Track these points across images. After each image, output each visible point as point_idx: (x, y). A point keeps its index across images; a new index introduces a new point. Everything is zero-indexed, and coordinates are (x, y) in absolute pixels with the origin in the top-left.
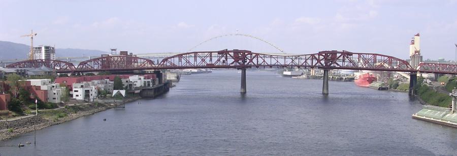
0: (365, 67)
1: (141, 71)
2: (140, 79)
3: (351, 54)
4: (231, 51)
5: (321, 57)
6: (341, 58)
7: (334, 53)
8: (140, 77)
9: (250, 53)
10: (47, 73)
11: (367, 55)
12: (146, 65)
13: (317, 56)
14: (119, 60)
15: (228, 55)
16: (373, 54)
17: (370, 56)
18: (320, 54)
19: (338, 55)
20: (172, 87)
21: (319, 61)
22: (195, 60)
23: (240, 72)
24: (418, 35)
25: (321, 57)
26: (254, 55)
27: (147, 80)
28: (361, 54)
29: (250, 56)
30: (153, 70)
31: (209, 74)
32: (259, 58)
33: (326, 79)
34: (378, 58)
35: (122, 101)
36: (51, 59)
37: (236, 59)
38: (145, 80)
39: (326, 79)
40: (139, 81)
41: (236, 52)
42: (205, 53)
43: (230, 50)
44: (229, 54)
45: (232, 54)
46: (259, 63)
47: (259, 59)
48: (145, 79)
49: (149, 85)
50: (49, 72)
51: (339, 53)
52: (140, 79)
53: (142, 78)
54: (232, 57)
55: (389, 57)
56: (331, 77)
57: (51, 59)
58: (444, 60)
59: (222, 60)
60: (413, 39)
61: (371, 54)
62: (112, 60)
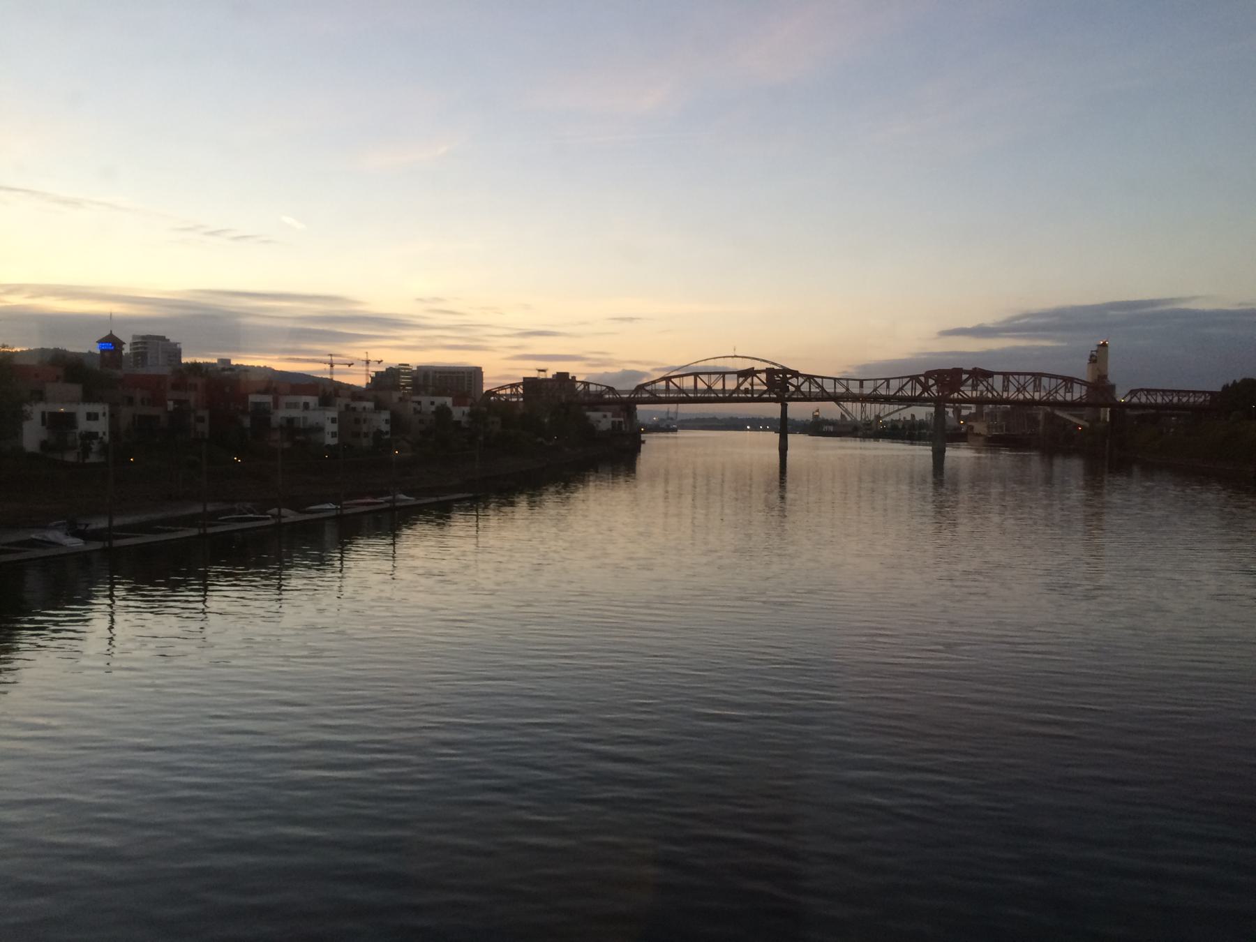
0: (990, 395)
2: (605, 416)
3: (989, 374)
4: (760, 372)
5: (931, 382)
6: (970, 382)
7: (957, 372)
13: (922, 379)
15: (671, 384)
16: (1033, 374)
18: (929, 375)
19: (965, 377)
20: (1211, 393)
21: (926, 388)
22: (1006, 388)
23: (779, 405)
25: (931, 382)
27: (617, 419)
28: (1013, 374)
36: (833, 391)
42: (878, 381)
43: (759, 369)
44: (908, 382)
51: (966, 372)
53: (609, 414)
57: (833, 391)
58: (753, 368)
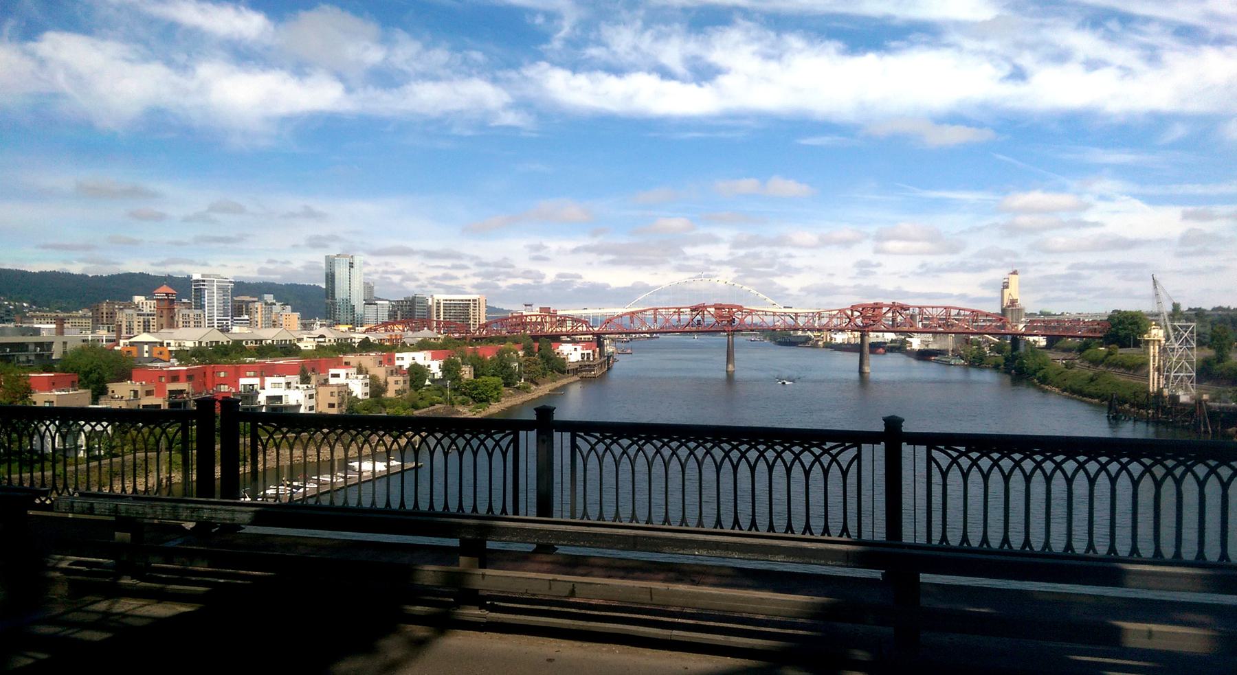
1: (573, 339)
7: (877, 307)
8: (576, 347)
9: (740, 308)
12: (580, 328)
14: (539, 320)
15: (705, 312)
17: (940, 310)
18: (853, 309)
24: (1015, 273)
27: (586, 352)
30: (591, 336)
31: (657, 340)
35: (294, 435)
40: (573, 352)
45: (712, 310)
49: (588, 358)
51: (887, 306)
53: (579, 348)
56: (516, 364)
60: (1006, 280)
61: (941, 307)
62: (528, 320)
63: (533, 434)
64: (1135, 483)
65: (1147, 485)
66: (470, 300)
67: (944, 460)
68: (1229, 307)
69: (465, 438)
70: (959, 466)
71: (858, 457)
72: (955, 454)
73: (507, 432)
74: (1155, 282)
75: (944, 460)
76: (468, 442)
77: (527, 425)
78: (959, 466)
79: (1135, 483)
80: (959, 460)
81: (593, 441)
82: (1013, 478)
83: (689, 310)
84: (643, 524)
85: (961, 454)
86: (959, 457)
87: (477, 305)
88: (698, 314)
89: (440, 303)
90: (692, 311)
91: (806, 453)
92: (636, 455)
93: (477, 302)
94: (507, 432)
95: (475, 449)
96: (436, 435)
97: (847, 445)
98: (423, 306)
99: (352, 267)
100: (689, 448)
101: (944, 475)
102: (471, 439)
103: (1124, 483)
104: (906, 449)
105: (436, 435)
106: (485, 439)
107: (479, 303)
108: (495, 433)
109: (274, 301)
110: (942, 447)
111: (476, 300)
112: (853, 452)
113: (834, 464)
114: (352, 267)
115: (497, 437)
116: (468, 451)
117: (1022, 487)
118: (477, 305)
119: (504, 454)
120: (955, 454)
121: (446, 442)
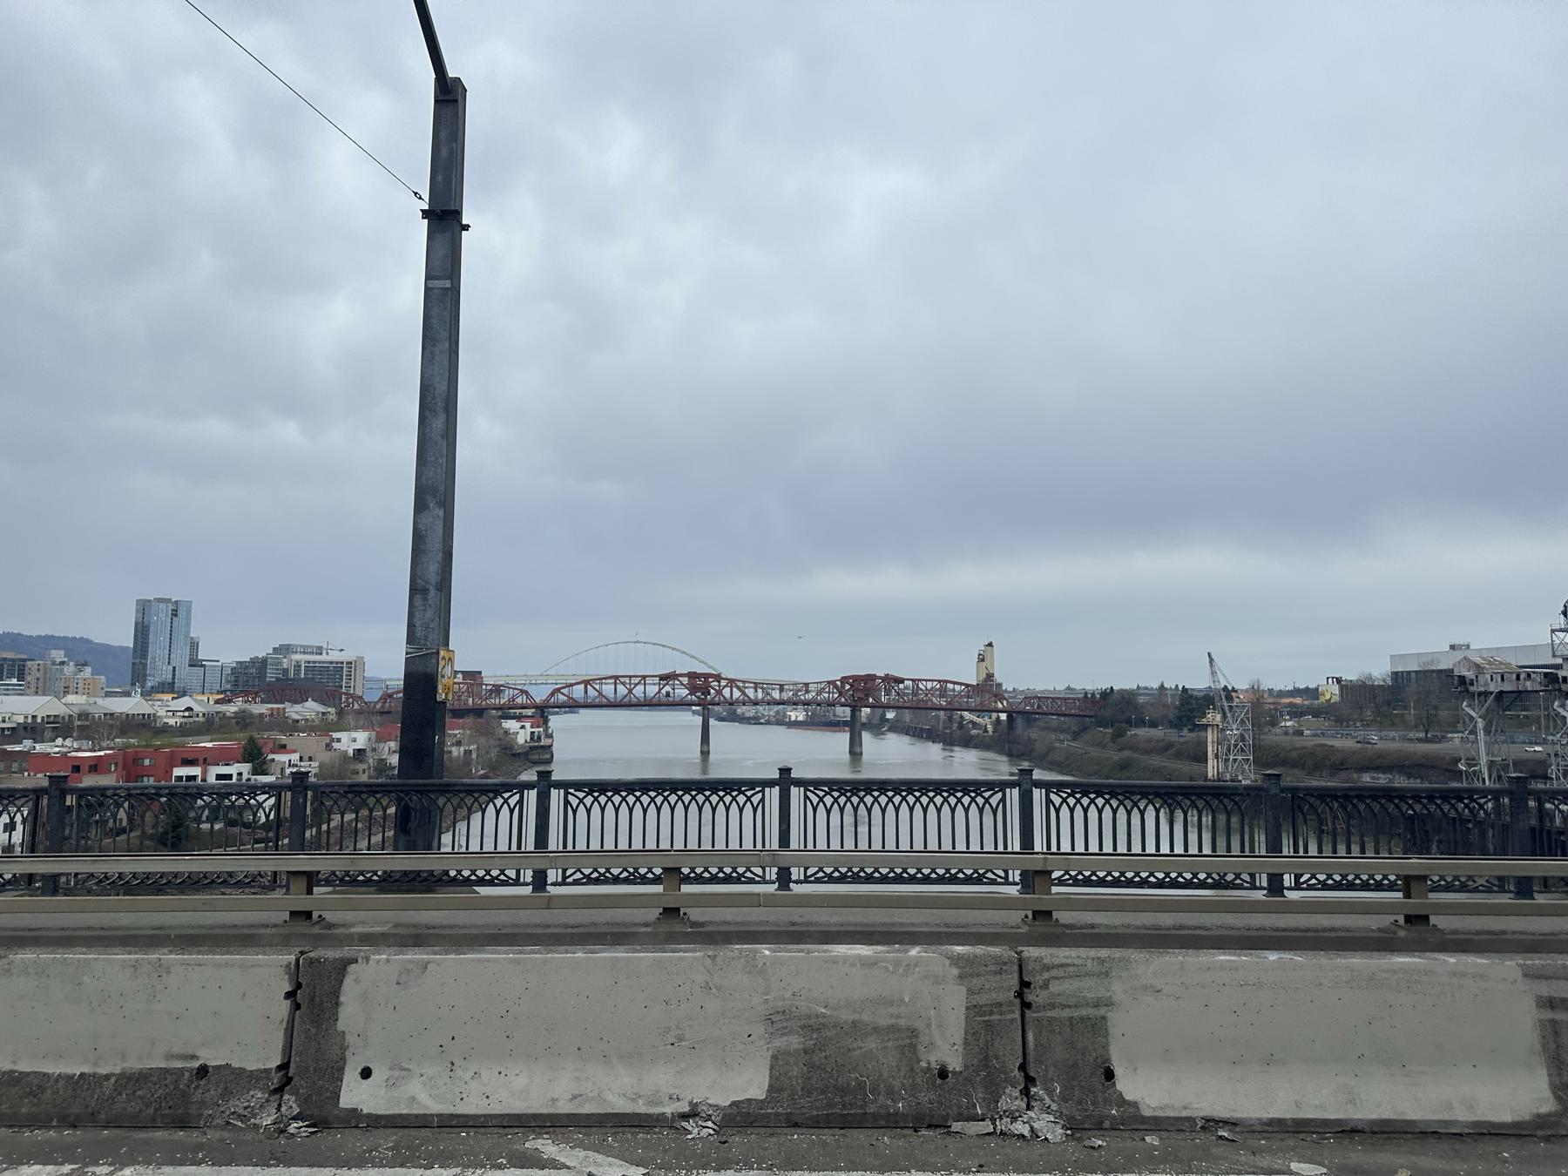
4: (681, 675)
9: (718, 678)
10: (320, 714)
11: (511, 690)
14: (938, 686)
18: (844, 680)
26: (723, 683)
28: (920, 680)
29: (716, 683)
32: (618, 686)
33: (615, 684)
34: (950, 686)
37: (693, 689)
38: (534, 730)
39: (615, 684)
41: (692, 676)
45: (685, 680)
46: (734, 698)
47: (620, 687)
48: (532, 727)
50: (323, 713)
51: (880, 678)
52: (523, 727)
54: (684, 686)
55: (940, 681)
59: (664, 691)
61: (936, 681)
63: (1016, 791)
64: (1100, 812)
65: (1107, 812)
66: (342, 663)
67: (1057, 800)
68: (1162, 686)
69: (873, 796)
70: (1068, 804)
71: (1003, 800)
72: (1064, 795)
73: (515, 791)
74: (1211, 660)
75: (1057, 800)
76: (876, 799)
77: (1012, 785)
78: (1068, 804)
79: (1100, 812)
80: (1068, 800)
81: (821, 794)
82: (1104, 811)
83: (658, 679)
84: (19, 854)
85: (1069, 795)
86: (1067, 797)
87: (353, 669)
88: (667, 684)
89: (300, 666)
90: (660, 680)
91: (952, 797)
92: (502, 806)
93: (353, 666)
94: (515, 791)
95: (883, 806)
96: (622, 793)
97: (982, 789)
98: (278, 669)
99: (176, 615)
100: (650, 797)
101: (815, 809)
102: (921, 796)
103: (1093, 812)
104: (794, 791)
105: (622, 793)
106: (710, 795)
107: (355, 667)
108: (746, 790)
109: (66, 659)
110: (1055, 790)
111: (351, 663)
112: (999, 795)
113: (918, 803)
114: (176, 615)
115: (987, 794)
116: (959, 808)
117: (1125, 817)
118: (353, 669)
119: (512, 811)
120: (1064, 795)
121: (952, 800)
